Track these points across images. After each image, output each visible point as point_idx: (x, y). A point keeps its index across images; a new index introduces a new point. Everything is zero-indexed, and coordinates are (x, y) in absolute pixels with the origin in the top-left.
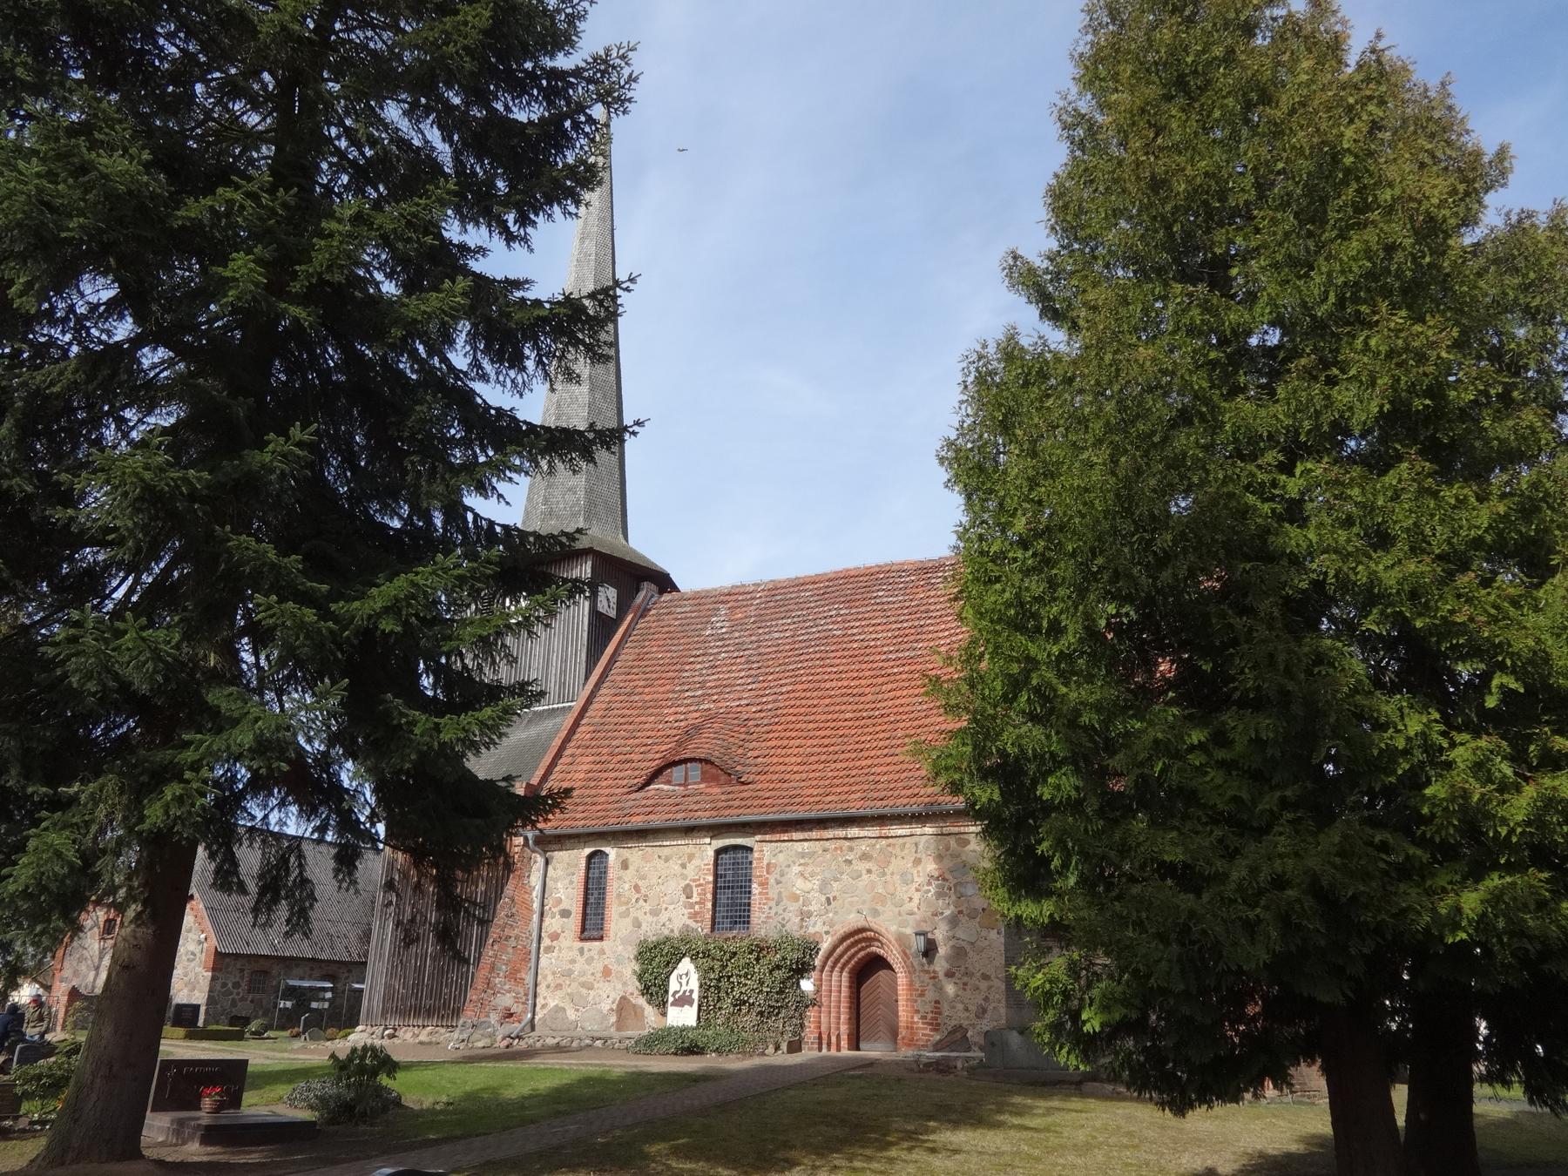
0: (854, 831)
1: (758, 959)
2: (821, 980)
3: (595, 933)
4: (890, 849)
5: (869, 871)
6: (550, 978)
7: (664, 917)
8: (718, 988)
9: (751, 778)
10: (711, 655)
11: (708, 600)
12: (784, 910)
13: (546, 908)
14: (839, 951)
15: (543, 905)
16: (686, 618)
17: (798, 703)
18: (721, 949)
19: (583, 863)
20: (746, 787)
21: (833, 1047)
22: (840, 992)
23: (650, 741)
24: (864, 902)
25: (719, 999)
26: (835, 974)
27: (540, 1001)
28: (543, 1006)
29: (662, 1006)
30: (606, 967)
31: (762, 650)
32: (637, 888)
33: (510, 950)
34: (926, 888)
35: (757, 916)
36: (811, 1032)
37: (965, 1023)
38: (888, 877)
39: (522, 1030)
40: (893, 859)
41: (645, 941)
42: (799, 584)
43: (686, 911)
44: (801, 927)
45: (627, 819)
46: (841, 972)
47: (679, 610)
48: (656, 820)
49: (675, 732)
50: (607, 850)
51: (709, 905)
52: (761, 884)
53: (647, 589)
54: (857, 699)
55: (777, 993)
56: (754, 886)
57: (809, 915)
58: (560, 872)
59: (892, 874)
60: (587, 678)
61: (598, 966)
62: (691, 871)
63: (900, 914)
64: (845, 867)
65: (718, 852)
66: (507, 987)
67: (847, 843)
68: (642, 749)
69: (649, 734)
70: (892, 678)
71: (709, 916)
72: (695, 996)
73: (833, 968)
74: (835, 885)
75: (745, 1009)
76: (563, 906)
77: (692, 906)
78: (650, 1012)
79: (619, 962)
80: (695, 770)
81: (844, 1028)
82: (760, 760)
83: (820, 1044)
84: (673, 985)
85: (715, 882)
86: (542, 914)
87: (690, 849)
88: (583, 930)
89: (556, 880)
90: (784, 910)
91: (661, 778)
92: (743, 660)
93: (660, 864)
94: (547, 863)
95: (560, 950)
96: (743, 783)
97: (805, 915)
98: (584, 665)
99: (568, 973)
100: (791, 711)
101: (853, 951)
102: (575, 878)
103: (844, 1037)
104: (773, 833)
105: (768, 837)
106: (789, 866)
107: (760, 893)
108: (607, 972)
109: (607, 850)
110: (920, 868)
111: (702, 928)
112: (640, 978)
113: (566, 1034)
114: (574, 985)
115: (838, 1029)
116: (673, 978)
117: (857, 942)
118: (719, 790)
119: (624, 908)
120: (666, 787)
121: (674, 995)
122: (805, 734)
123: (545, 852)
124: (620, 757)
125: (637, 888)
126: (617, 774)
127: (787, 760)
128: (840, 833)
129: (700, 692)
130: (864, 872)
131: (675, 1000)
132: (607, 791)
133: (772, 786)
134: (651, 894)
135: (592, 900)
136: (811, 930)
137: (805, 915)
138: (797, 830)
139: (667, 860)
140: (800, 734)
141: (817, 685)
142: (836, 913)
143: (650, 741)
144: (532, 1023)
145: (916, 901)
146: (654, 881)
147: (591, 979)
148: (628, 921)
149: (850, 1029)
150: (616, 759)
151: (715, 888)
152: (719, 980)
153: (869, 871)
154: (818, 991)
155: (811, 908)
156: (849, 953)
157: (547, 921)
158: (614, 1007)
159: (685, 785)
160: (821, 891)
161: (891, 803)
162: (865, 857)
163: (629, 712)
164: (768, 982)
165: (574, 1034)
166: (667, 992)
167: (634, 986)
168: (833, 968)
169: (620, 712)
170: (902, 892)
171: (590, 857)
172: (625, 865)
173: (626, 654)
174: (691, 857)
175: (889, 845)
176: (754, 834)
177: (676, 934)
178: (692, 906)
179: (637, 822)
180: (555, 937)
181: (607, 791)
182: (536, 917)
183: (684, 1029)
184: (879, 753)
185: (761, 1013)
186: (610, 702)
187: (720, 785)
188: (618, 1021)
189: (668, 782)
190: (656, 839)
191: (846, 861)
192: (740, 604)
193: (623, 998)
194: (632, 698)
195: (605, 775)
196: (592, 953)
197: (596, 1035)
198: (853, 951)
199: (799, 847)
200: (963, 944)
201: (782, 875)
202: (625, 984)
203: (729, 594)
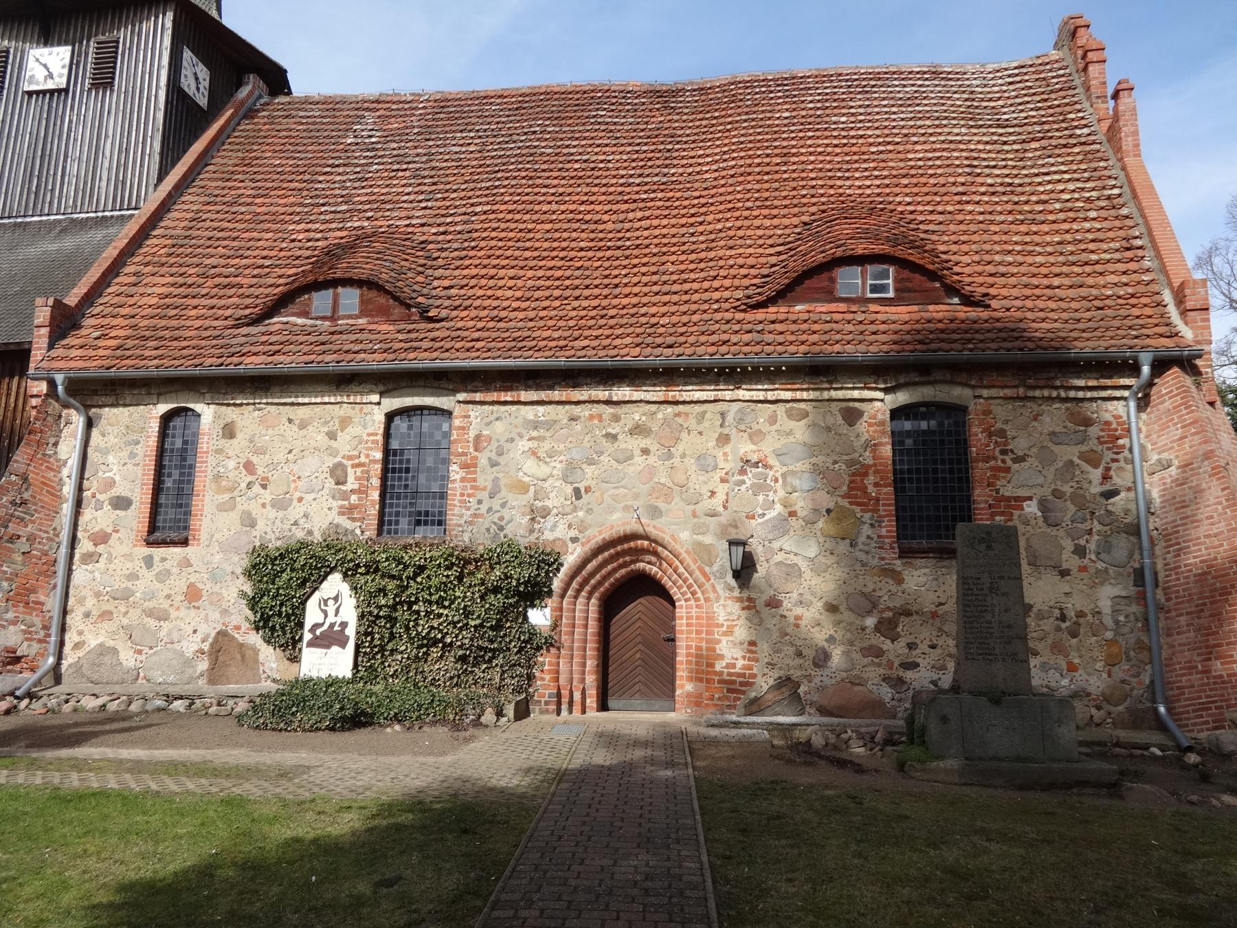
0: (622, 392)
1: (460, 578)
2: (561, 609)
3: (174, 535)
4: (680, 420)
5: (646, 452)
6: (90, 603)
7: (296, 511)
8: (392, 620)
9: (444, 313)
10: (357, 165)
11: (345, 106)
12: (503, 505)
13: (87, 494)
14: (590, 567)
15: (80, 489)
16: (314, 123)
17: (503, 226)
18: (399, 561)
19: (155, 426)
20: (438, 325)
21: (577, 707)
22: (586, 626)
23: (267, 263)
24: (636, 496)
25: (392, 637)
26: (581, 600)
27: (71, 638)
28: (77, 646)
29: (291, 648)
30: (191, 586)
31: (434, 164)
32: (249, 467)
33: (18, 558)
34: (737, 478)
35: (457, 514)
36: (545, 687)
37: (796, 674)
38: (676, 461)
39: (38, 682)
40: (684, 435)
41: (263, 547)
42: (485, 98)
43: (335, 504)
44: (532, 531)
45: (235, 360)
46: (589, 598)
47: (302, 114)
48: (288, 362)
49: (309, 253)
50: (198, 407)
51: (375, 495)
52: (465, 466)
53: (250, 88)
54: (593, 227)
55: (491, 628)
56: (454, 467)
57: (545, 513)
58: (112, 440)
59: (683, 456)
60: (160, 179)
61: (178, 584)
62: (344, 443)
63: (694, 515)
64: (606, 444)
65: (390, 417)
66: (10, 615)
67: (609, 410)
68: (256, 272)
69: (265, 253)
70: (641, 205)
71: (374, 511)
72: (351, 632)
73: (578, 591)
74: (589, 470)
75: (435, 652)
76: (117, 491)
77: (345, 496)
78: (270, 658)
79: (214, 579)
80: (350, 298)
81: (591, 679)
82: (453, 292)
83: (559, 704)
84: (312, 615)
85: (385, 461)
86: (79, 503)
87: (345, 410)
88: (153, 527)
89: (106, 452)
90: (503, 505)
91: (292, 308)
92: (408, 174)
93: (292, 431)
94: (90, 424)
95: (110, 559)
96: (431, 320)
97: (537, 514)
98: (157, 158)
99: (125, 595)
100: (494, 234)
101: (610, 567)
102: (139, 450)
103: (592, 693)
104: (488, 390)
105: (478, 396)
106: (512, 440)
107: (463, 480)
108: (193, 595)
109: (198, 407)
110: (728, 449)
111: (363, 529)
112: (253, 603)
113: (117, 689)
114: (135, 614)
115: (583, 680)
116: (312, 606)
117: (618, 555)
118: (391, 328)
119: (226, 496)
120: (300, 321)
121: (312, 630)
122: (522, 264)
123: (87, 407)
124: (217, 280)
125: (249, 467)
126: (214, 301)
127: (499, 293)
128: (601, 393)
129: (344, 207)
130: (637, 452)
131: (316, 638)
132: (198, 323)
133: (480, 325)
134: (275, 477)
135: (168, 483)
136: (548, 536)
137: (537, 514)
138: (527, 388)
139: (303, 426)
140: (514, 263)
141: (529, 207)
142: (590, 511)
143: (267, 263)
144: (56, 675)
145: (721, 497)
146: (280, 456)
147: (165, 604)
148: (234, 516)
149: (597, 680)
150: (210, 283)
151: (385, 470)
152: (394, 608)
153: (646, 452)
154: (555, 626)
155: (549, 503)
156: (604, 572)
157: (87, 515)
158: (206, 647)
159: (333, 318)
160: (565, 478)
161: (688, 351)
162: (638, 430)
163: (231, 226)
164: (478, 610)
165: (133, 689)
166: (300, 625)
167: (240, 617)
168: (578, 591)
169: (216, 224)
170: (699, 482)
171: (166, 419)
172: (229, 432)
173: (223, 157)
174: (345, 422)
175: (678, 415)
176: (454, 391)
177: (317, 537)
178: (345, 496)
179: (254, 364)
180: (101, 538)
181: (198, 323)
182: (67, 509)
183: (332, 682)
184: (646, 289)
185: (463, 659)
186: (198, 211)
187: (390, 321)
188: (212, 668)
189: (305, 314)
190: (284, 392)
191: (608, 435)
192: (393, 113)
193: (222, 634)
194: (234, 209)
195: (195, 302)
196: (167, 565)
197: (172, 690)
198: (610, 567)
199: (529, 412)
200: (796, 560)
201: (500, 454)
202: (225, 612)
203: (378, 102)
